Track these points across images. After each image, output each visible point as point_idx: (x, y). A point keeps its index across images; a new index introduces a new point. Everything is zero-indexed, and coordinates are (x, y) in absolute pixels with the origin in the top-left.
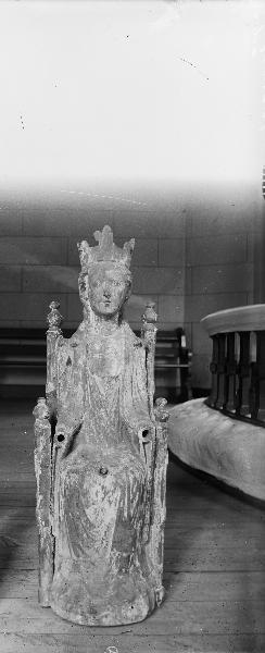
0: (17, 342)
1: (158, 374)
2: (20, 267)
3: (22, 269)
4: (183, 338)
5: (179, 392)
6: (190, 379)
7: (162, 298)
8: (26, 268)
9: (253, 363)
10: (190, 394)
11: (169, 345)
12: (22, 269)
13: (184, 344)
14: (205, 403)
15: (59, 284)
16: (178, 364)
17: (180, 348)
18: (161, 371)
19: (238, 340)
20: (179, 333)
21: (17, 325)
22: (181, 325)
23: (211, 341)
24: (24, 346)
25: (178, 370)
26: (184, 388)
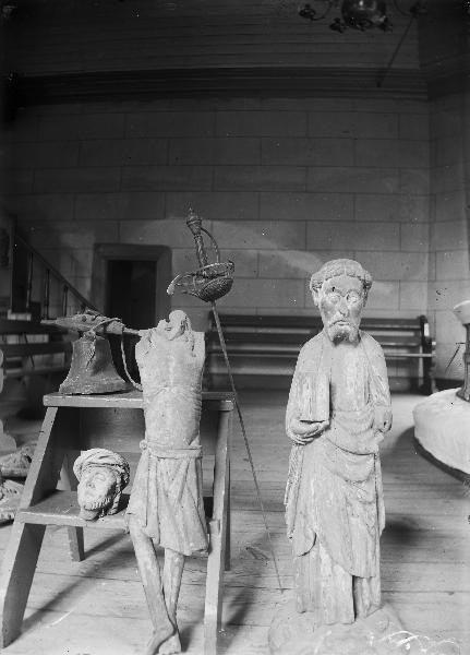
0: (252, 330)
1: (391, 363)
2: (255, 252)
3: (259, 255)
4: (426, 326)
5: (421, 383)
6: (432, 369)
7: (402, 284)
8: (262, 252)
9: (51, 339)
10: (433, 384)
11: (411, 334)
12: (259, 255)
13: (427, 333)
14: (457, 394)
15: (296, 270)
16: (421, 354)
17: (423, 337)
18: (392, 361)
19: (230, 330)
20: (422, 320)
21: (252, 312)
22: (424, 313)
23: (465, 330)
24: (259, 334)
25: (421, 361)
26: (426, 377)
